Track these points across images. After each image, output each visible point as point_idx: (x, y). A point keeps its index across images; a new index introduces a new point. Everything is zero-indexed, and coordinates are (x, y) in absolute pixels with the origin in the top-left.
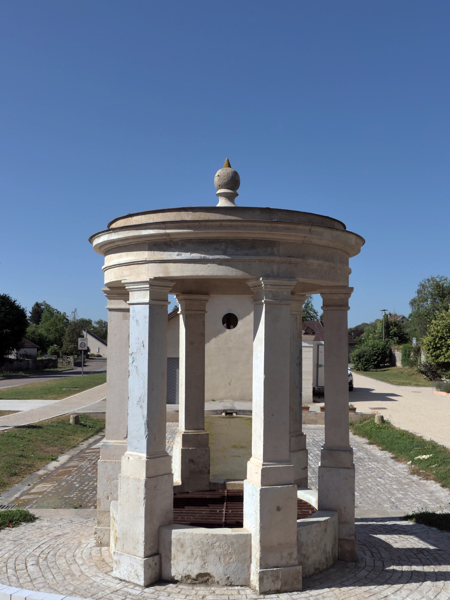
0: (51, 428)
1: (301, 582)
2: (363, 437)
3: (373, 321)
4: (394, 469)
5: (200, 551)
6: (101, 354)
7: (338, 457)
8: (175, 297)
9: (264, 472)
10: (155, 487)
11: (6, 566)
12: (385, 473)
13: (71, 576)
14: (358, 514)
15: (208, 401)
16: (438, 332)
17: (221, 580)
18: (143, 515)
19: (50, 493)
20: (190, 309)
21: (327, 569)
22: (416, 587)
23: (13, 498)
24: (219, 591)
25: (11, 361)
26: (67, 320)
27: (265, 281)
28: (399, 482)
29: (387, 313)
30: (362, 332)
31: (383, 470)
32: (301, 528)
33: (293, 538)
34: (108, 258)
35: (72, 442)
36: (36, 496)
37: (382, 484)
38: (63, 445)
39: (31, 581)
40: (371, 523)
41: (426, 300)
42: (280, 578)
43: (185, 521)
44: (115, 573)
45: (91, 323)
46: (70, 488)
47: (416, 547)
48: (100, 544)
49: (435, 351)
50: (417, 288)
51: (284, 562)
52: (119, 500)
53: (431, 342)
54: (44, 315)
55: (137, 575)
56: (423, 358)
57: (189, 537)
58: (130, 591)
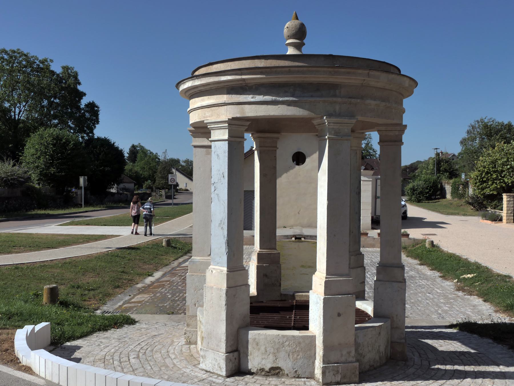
0: (147, 249)
1: (358, 376)
2: (415, 259)
3: (427, 159)
4: (442, 286)
5: (272, 349)
6: (188, 188)
7: (391, 273)
8: (251, 135)
9: (327, 284)
10: (234, 296)
11: (113, 359)
12: (434, 289)
13: (166, 367)
14: (408, 322)
15: (279, 227)
16: (485, 167)
17: (290, 373)
18: (225, 318)
19: (147, 302)
20: (264, 146)
21: (381, 366)
22: (457, 383)
23: (117, 306)
24: (288, 381)
25: (113, 194)
26: (159, 159)
27: (328, 119)
28: (446, 297)
29: (439, 151)
30: (416, 169)
31: (432, 286)
32: (358, 331)
33: (352, 339)
34: (192, 101)
35: (165, 261)
36: (136, 304)
37: (430, 299)
38: (158, 263)
39: (133, 371)
40: (420, 330)
41: (475, 139)
42: (340, 372)
43: (260, 324)
44: (202, 366)
45: (179, 162)
46: (164, 298)
47: (459, 350)
48: (190, 342)
49: (481, 184)
50: (467, 128)
51: (343, 359)
52: (204, 306)
53: (478, 177)
54: (138, 155)
55: (220, 367)
56: (471, 191)
57: (263, 337)
58: (214, 380)
